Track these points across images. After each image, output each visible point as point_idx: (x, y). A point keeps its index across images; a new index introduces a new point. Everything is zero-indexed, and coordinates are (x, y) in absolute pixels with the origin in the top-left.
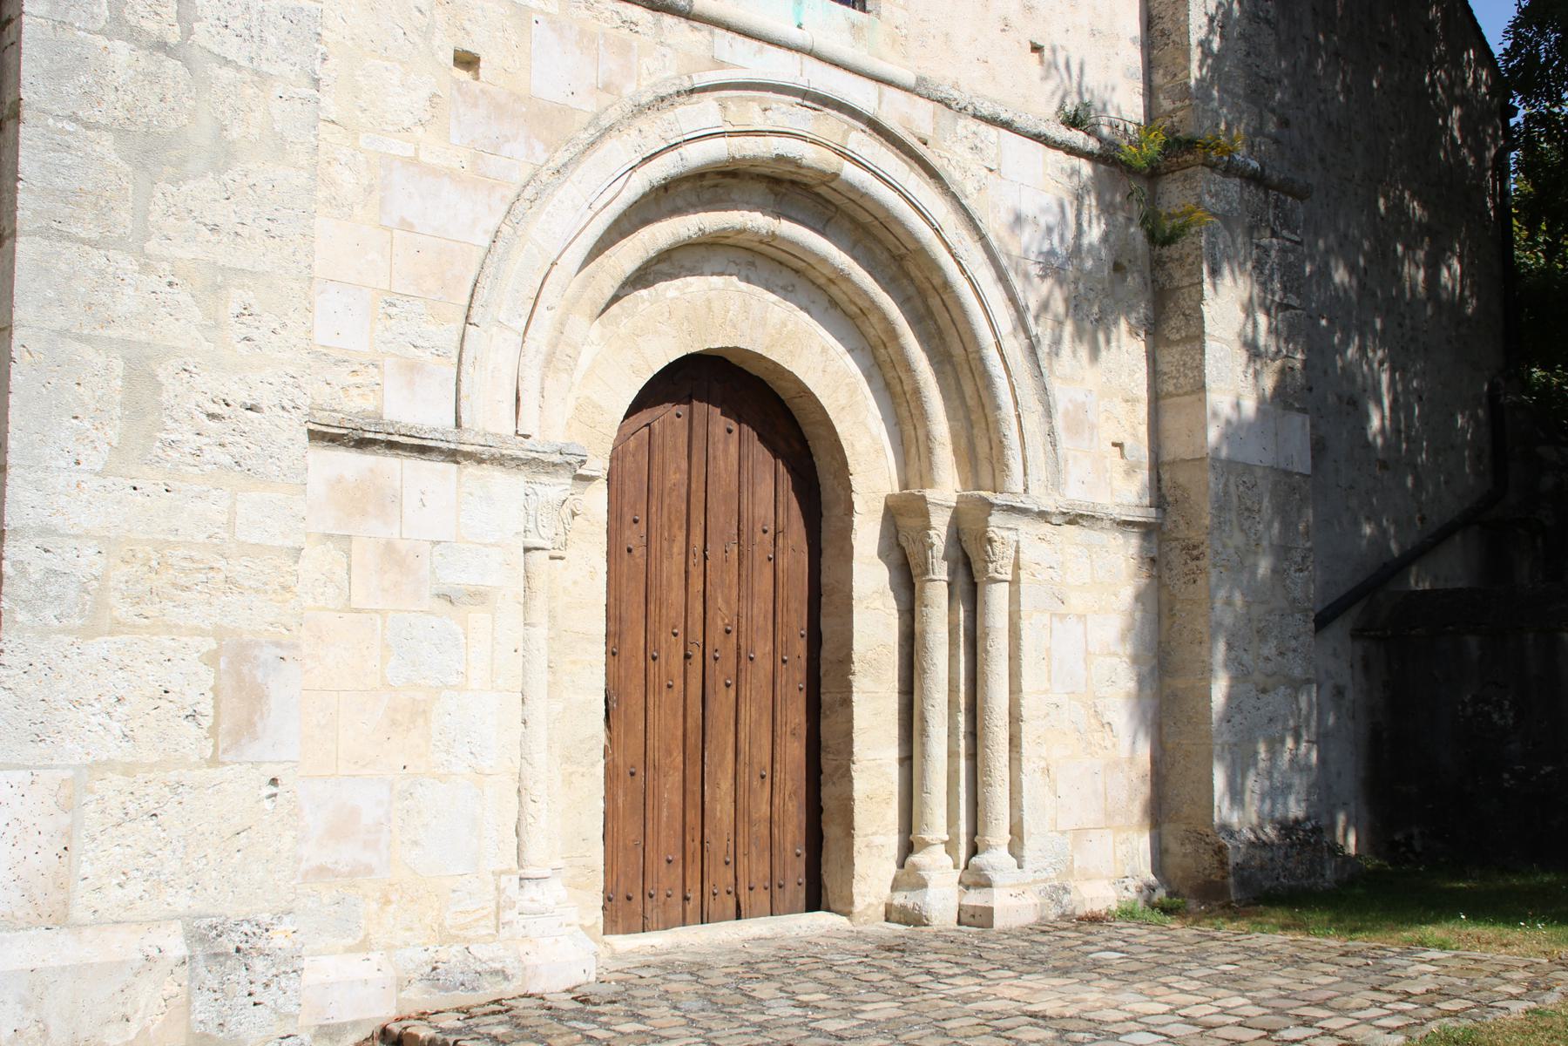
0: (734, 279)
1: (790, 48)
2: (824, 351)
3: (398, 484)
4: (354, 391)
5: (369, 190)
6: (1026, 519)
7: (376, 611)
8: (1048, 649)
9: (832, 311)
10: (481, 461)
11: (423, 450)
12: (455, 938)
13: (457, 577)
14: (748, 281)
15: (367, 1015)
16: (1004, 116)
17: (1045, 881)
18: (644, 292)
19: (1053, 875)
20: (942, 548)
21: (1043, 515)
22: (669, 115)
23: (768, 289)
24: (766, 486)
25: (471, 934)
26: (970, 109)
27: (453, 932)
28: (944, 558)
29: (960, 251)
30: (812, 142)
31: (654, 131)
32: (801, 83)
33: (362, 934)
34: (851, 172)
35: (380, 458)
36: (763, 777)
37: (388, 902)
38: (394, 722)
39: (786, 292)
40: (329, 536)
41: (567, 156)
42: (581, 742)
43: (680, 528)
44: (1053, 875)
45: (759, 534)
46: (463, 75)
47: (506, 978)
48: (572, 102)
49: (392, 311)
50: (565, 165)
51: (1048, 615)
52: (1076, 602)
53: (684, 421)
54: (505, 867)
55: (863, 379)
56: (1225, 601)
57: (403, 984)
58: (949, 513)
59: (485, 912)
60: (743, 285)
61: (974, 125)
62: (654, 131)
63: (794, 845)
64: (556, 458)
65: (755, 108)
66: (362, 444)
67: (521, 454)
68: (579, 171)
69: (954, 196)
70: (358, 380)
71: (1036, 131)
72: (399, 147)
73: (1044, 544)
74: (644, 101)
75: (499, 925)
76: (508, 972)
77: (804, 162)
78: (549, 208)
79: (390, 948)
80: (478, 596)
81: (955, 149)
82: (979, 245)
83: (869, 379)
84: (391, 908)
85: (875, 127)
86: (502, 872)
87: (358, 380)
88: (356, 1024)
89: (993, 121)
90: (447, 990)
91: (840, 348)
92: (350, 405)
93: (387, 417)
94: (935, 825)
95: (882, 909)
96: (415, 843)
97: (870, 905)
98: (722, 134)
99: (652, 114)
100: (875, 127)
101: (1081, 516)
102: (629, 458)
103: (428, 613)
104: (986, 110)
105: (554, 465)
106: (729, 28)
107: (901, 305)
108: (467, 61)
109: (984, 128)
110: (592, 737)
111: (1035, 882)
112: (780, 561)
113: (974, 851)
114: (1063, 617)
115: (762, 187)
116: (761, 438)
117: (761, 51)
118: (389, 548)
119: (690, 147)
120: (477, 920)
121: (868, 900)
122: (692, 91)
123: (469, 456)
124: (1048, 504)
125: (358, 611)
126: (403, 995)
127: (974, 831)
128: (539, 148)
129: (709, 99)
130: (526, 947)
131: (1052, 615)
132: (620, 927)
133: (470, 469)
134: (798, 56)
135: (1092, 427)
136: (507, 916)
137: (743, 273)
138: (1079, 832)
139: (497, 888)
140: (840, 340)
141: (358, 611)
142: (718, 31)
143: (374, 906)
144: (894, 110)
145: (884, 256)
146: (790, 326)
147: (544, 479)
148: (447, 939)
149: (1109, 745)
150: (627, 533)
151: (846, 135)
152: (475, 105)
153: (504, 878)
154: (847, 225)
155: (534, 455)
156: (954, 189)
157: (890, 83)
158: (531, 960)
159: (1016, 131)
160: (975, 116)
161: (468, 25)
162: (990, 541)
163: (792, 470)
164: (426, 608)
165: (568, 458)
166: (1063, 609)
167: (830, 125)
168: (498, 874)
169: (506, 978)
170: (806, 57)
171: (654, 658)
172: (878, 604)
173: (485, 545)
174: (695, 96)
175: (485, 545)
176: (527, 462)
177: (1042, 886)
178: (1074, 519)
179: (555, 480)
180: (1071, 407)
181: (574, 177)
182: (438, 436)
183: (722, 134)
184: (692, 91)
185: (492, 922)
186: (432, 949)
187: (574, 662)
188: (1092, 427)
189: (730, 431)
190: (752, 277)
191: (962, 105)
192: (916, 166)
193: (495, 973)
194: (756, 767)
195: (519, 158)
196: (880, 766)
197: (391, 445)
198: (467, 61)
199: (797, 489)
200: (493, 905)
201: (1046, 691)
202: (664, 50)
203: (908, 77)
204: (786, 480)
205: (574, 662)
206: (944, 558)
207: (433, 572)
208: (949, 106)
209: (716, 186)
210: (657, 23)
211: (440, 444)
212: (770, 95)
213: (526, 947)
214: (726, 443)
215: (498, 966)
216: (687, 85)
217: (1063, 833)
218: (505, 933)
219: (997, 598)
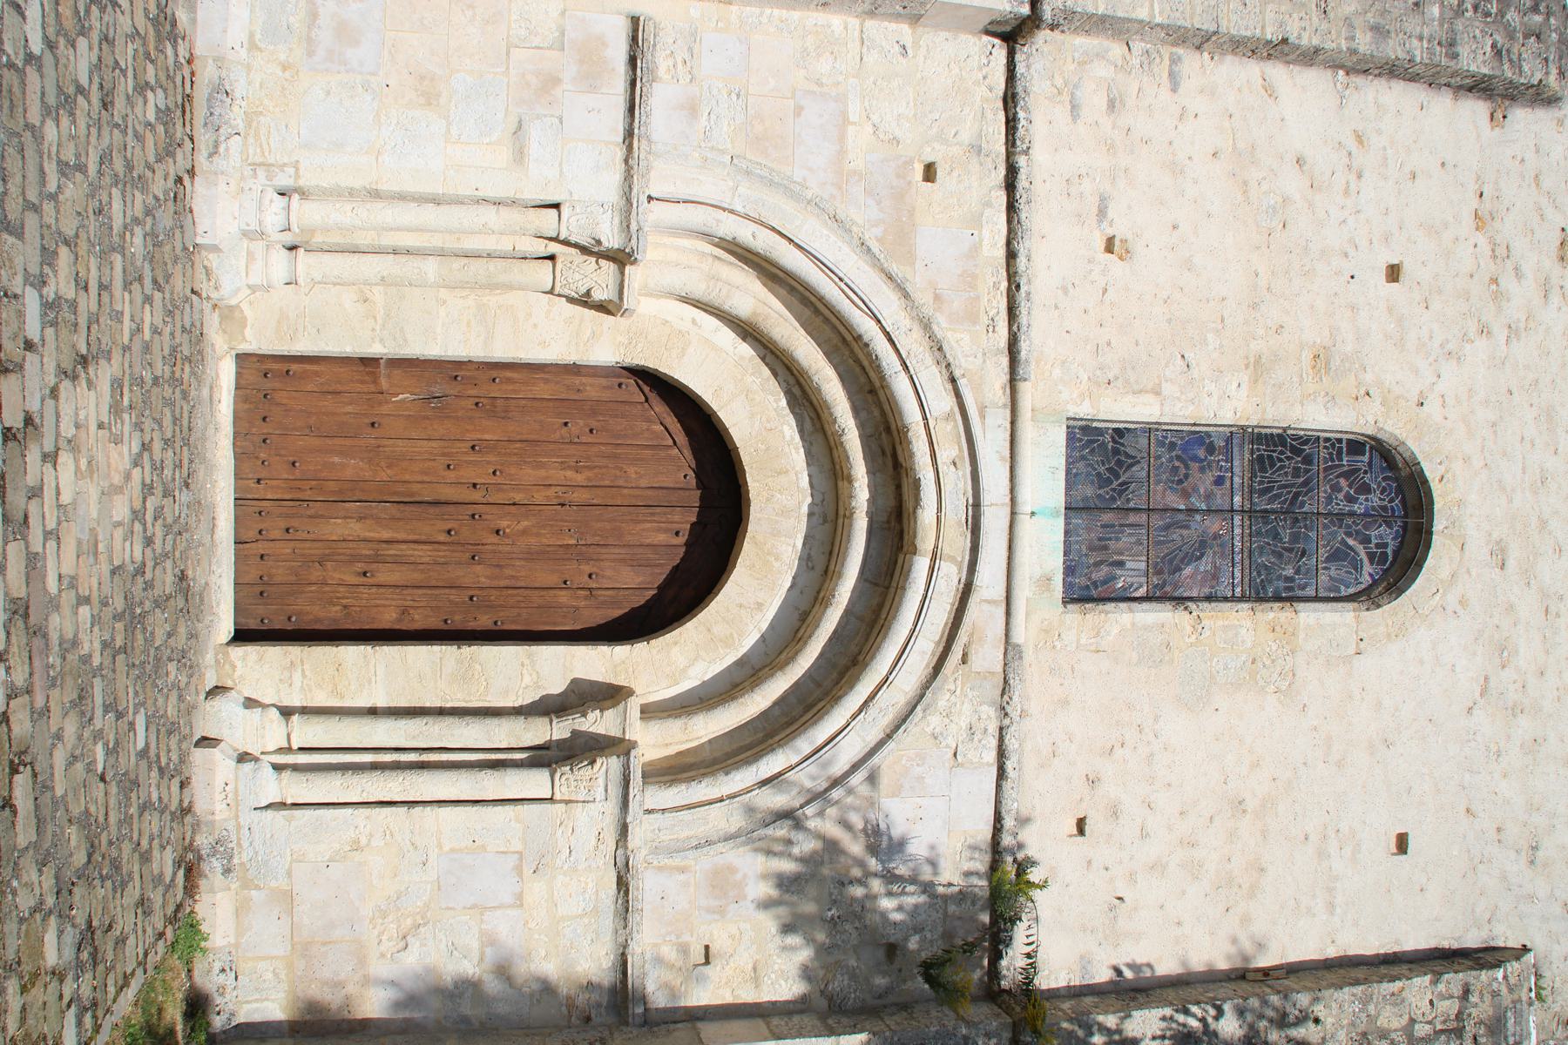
0: (809, 500)
1: (1012, 490)
2: (760, 606)
4: (670, 62)
5: (819, 83)
6: (617, 811)
8: (483, 847)
9: (796, 616)
10: (626, 161)
11: (631, 109)
12: (249, 125)
13: (534, 132)
14: (810, 515)
15: (199, 32)
16: (1009, 765)
17: (239, 844)
18: (784, 402)
19: (245, 858)
20: (583, 728)
21: (624, 830)
22: (929, 360)
23: (806, 538)
24: (635, 583)
25: (251, 140)
26: (1007, 722)
27: (254, 124)
28: (574, 732)
29: (873, 711)
30: (936, 518)
31: (913, 343)
32: (987, 498)
33: (262, 46)
34: (921, 565)
36: (365, 574)
37: (284, 69)
38: (422, 78)
39: (806, 560)
40: (563, 34)
41: (875, 250)
42: (402, 330)
43: (589, 479)
44: (245, 858)
45: (587, 569)
46: (919, 170)
47: (211, 155)
48: (919, 265)
49: (734, 97)
50: (869, 250)
51: (519, 847)
52: (536, 890)
53: (682, 483)
55: (740, 655)
57: (220, 61)
58: (619, 734)
60: (805, 509)
61: (993, 728)
62: (913, 343)
63: (299, 614)
64: (634, 227)
65: (954, 453)
66: (632, 61)
67: (635, 191)
68: (867, 268)
69: (922, 696)
70: (680, 65)
71: (1003, 813)
72: (854, 110)
73: (594, 842)
74: (935, 327)
75: (255, 166)
76: (215, 158)
77: (919, 511)
78: (833, 238)
79: (249, 68)
80: (520, 155)
81: (962, 706)
82: (882, 735)
83: (740, 663)
85: (967, 591)
87: (680, 65)
88: (194, 21)
89: (1002, 754)
90: (208, 100)
91: (764, 626)
92: (662, 60)
94: (308, 732)
95: (229, 684)
96: (328, 93)
97: (234, 667)
98: (925, 418)
99: (926, 342)
100: (967, 591)
101: (627, 892)
102: (645, 425)
104: (1011, 743)
106: (1013, 423)
107: (809, 675)
108: (930, 173)
109: (994, 743)
111: (239, 827)
112: (563, 593)
113: (278, 768)
114: (519, 870)
115: (891, 502)
116: (676, 569)
117: (1002, 459)
118: (556, 81)
119: (907, 381)
121: (239, 664)
122: (953, 380)
123: (630, 148)
124: (636, 838)
125: (508, 53)
127: (296, 768)
128: (878, 231)
129: (949, 403)
131: (520, 853)
132: (240, 392)
133: (620, 154)
134: (1007, 500)
135: (721, 912)
136: (261, 173)
137: (816, 509)
138: (287, 899)
139: (285, 165)
140: (772, 626)
141: (508, 53)
142: (1008, 412)
143: (283, 57)
144: (984, 614)
145: (854, 649)
146: (777, 564)
147: (617, 221)
148: (249, 118)
149: (382, 948)
150: (581, 422)
151: (952, 559)
152: (898, 176)
153: (292, 171)
154: (875, 602)
156: (929, 694)
157: (1008, 613)
159: (999, 787)
160: (1001, 729)
161: (955, 174)
162: (592, 762)
163: (649, 605)
166: (527, 872)
167: (956, 542)
168: (296, 165)
169: (211, 155)
170: (1008, 510)
171: (473, 447)
172: (527, 680)
174: (949, 386)
176: (629, 201)
177: (234, 838)
178: (622, 884)
180: (739, 876)
181: (861, 263)
183: (925, 418)
184: (953, 380)
186: (243, 104)
187: (468, 323)
188: (721, 912)
189: (677, 534)
190: (815, 518)
191: (1008, 709)
192: (941, 649)
193: (216, 145)
194: (374, 566)
195: (864, 214)
196: (370, 682)
197: (633, 83)
198: (930, 173)
199: (634, 612)
200: (272, 161)
201: (440, 846)
202: (980, 355)
203: (1019, 636)
204: (639, 600)
205: (468, 323)
206: (574, 732)
207: (538, 117)
208: (1003, 694)
209: (883, 453)
210: (999, 351)
212: (968, 469)
214: (666, 531)
215: (222, 149)
216: (957, 373)
217: (289, 874)
218: (248, 172)
219: (535, 782)
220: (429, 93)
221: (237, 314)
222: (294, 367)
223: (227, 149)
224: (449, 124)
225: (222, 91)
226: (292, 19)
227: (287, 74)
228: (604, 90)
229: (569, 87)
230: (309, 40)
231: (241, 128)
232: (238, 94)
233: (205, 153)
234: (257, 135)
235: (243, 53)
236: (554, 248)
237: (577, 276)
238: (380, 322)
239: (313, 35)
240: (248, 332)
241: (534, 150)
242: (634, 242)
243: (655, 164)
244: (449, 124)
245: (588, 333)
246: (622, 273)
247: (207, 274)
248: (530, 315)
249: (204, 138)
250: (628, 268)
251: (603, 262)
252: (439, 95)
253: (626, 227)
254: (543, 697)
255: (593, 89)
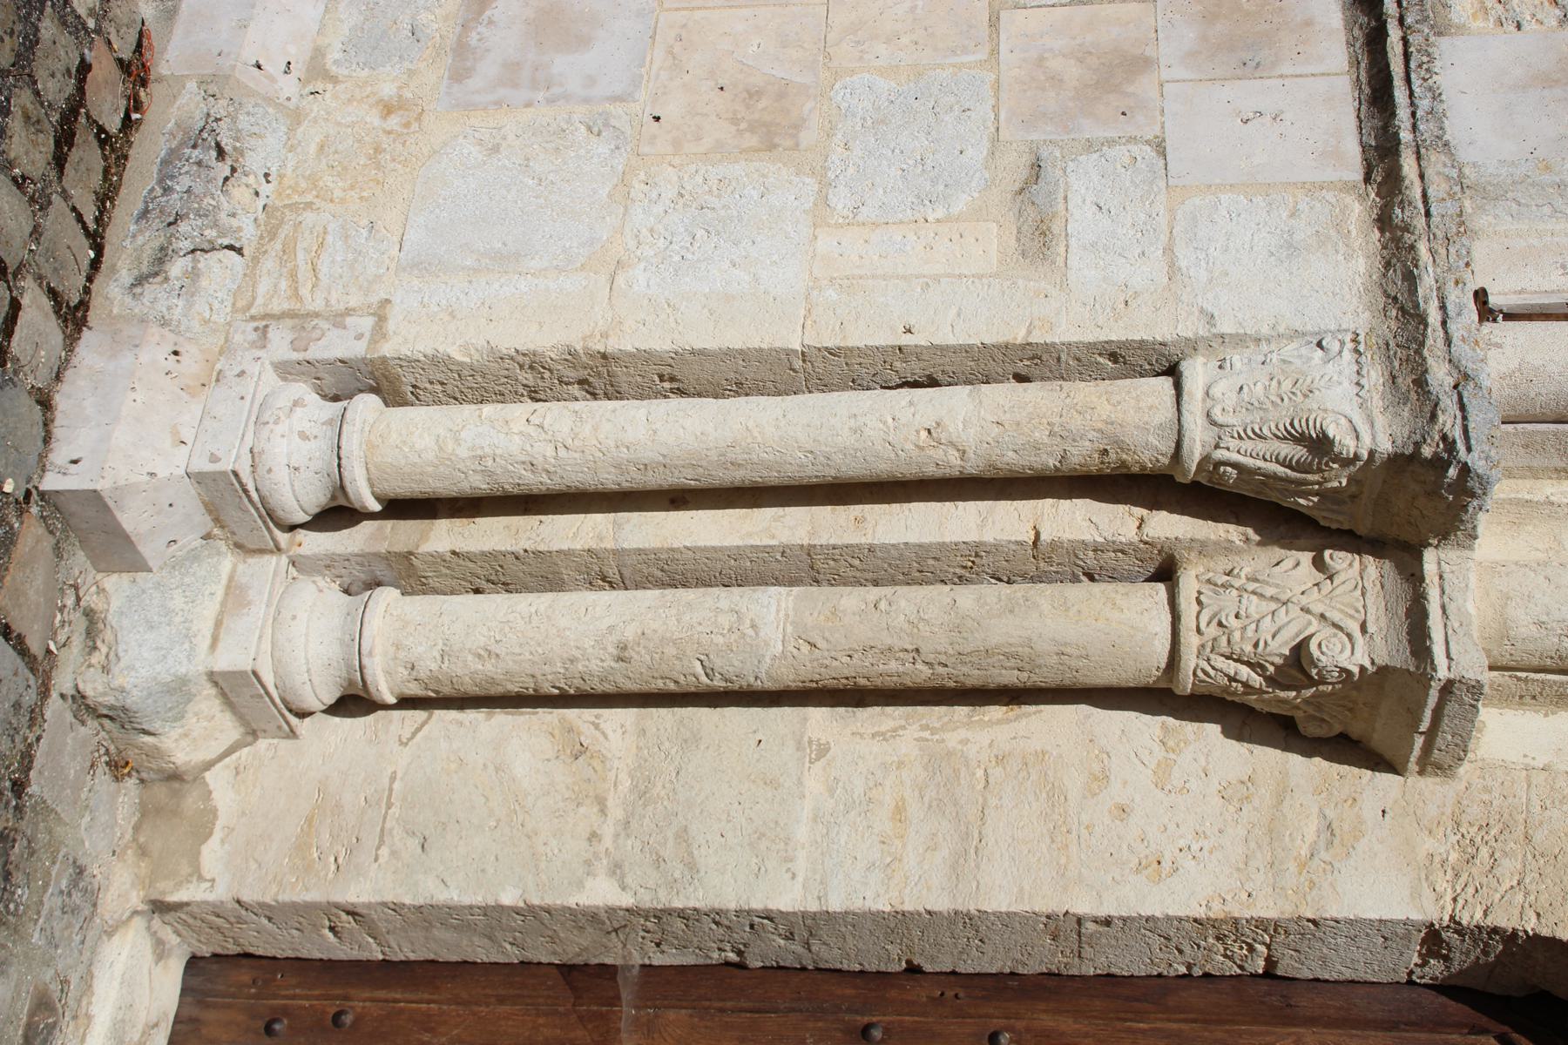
3: (1286, 69)
7: (995, 52)
10: (1384, 221)
11: (1378, 94)
13: (1082, 189)
25: (269, 264)
33: (342, 72)
35: (1342, 37)
37: (388, 110)
38: (753, 94)
42: (683, 835)
47: (140, 281)
54: (391, 326)
56: (1363, 65)
59: (305, 292)
64: (1440, 376)
67: (1426, 284)
76: (151, 289)
80: (1039, 238)
84: (374, 119)
86: (381, 319)
90: (165, 162)
93: (1443, 45)
103: (995, 139)
105: (1421, 383)
110: (692, 866)
118: (1139, 64)
120: (293, 276)
125: (994, 22)
126: (192, 85)
130: (191, 363)
133: (1358, 211)
139: (349, 312)
141: (994, 22)
143: (388, 90)
147: (1375, 376)
153: (367, 323)
155: (1434, 317)
158: (154, 352)
164: (1004, 134)
165: (1449, 403)
169: (140, 281)
173: (1169, 250)
175: (1169, 250)
176: (1410, 316)
179: (1377, 403)
182: (1424, 104)
185: (276, 307)
186: (265, 189)
187: (899, 812)
193: (162, 257)
197: (1375, 40)
200: (317, 305)
205: (899, 812)
207: (1090, 146)
211: (1403, 113)
213: (191, 363)
215: (177, 268)
218: (244, 333)
220: (768, 122)
221: (191, 802)
222: (362, 1002)
223: (194, 274)
224: (825, 185)
225: (213, 146)
226: (424, 17)
227: (394, 122)
228: (1286, 69)
229: (1179, 72)
230: (461, 49)
231: (248, 234)
232: (254, 162)
233: (126, 277)
234: (288, 250)
235: (288, 87)
236: (1168, 526)
237: (1253, 606)
238: (616, 812)
239: (473, 38)
240: (212, 854)
241: (1081, 220)
242: (1448, 419)
243: (1481, 221)
244: (825, 185)
245: (1311, 828)
246: (1414, 578)
247: (91, 633)
248: (1103, 778)
249: (129, 240)
250: (1430, 558)
251: (1338, 559)
252: (797, 127)
253: (1411, 385)
254: (1310, 756)
255: (1250, 68)
